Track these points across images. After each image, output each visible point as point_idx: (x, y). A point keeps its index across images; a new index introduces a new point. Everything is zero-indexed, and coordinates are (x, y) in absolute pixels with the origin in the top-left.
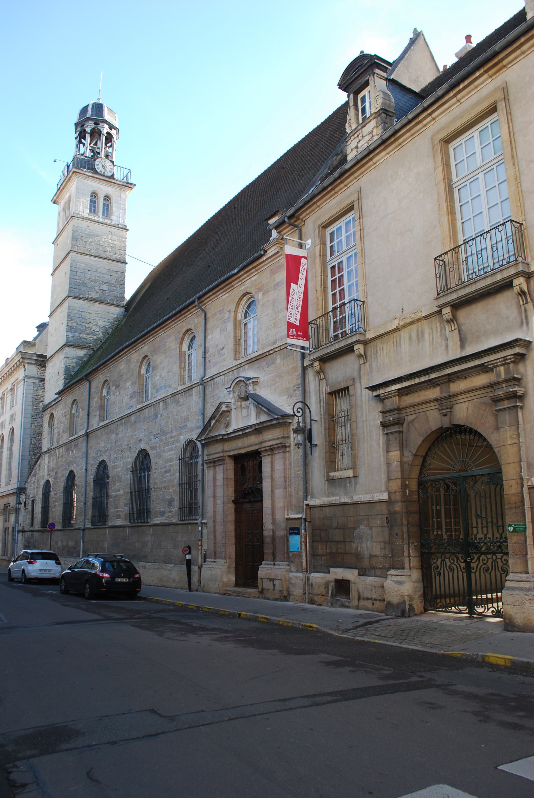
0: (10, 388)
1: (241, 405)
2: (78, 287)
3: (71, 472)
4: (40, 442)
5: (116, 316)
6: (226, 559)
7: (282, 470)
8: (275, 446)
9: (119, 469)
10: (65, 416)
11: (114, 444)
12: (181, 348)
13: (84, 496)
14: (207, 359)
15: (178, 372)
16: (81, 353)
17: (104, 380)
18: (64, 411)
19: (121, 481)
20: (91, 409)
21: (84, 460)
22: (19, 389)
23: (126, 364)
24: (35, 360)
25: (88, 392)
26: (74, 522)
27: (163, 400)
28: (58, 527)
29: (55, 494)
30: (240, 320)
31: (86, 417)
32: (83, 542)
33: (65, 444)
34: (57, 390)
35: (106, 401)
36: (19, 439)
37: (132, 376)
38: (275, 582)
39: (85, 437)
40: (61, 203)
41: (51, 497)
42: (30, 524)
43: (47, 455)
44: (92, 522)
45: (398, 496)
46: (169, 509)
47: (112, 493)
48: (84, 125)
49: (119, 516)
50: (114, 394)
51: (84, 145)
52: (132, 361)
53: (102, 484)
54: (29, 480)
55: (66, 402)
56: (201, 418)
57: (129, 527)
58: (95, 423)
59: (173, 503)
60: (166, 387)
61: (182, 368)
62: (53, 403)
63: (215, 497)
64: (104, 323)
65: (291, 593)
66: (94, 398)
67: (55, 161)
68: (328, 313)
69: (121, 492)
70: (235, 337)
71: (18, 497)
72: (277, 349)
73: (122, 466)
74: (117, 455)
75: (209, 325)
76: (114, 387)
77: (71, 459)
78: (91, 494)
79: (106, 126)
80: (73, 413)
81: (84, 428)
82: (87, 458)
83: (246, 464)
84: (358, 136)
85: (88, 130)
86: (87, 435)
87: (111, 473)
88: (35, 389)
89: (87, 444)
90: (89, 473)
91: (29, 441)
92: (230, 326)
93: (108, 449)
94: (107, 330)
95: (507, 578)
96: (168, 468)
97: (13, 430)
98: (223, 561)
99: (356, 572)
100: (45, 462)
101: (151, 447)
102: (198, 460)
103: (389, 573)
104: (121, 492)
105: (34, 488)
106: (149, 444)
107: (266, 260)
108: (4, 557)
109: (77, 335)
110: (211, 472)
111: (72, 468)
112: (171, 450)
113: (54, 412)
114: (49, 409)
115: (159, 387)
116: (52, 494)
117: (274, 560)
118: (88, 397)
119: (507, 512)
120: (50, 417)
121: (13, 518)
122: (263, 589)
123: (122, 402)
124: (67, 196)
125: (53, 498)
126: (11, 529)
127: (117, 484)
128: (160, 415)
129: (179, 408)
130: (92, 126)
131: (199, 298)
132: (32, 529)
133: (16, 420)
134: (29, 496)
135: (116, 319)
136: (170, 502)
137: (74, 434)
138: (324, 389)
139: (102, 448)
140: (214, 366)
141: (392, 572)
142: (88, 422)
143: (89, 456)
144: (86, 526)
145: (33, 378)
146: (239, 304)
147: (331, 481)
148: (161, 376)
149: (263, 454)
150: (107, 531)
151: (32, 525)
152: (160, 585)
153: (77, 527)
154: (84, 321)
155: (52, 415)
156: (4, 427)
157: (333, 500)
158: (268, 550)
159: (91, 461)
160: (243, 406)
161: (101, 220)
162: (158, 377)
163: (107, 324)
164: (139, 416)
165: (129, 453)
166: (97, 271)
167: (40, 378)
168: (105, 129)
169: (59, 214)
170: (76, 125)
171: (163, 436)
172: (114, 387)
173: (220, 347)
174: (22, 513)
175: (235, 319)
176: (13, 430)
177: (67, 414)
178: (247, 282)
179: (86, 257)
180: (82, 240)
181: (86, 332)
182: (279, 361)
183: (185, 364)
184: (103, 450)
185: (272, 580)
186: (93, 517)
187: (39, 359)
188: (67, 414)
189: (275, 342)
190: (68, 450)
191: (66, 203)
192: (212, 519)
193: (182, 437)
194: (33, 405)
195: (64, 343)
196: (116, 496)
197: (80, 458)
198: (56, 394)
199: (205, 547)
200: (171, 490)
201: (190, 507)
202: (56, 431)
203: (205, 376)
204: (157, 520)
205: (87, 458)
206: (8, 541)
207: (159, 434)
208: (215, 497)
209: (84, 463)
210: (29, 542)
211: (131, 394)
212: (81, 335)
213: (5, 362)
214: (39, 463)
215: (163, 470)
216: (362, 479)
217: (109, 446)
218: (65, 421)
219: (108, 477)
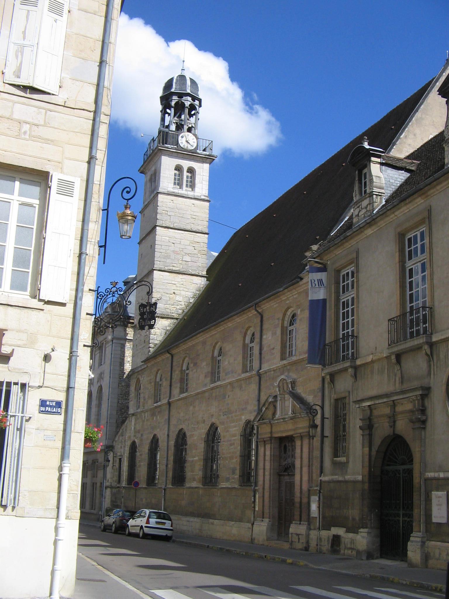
2: (163, 260)
3: (155, 436)
4: (126, 401)
10: (151, 383)
13: (166, 459)
15: (241, 361)
18: (149, 378)
21: (167, 426)
22: (107, 349)
25: (170, 365)
26: (157, 482)
27: (231, 384)
28: (143, 485)
29: (141, 455)
30: (287, 327)
31: (169, 387)
32: (164, 500)
38: (300, 536)
39: (168, 406)
43: (134, 418)
44: (172, 483)
45: (366, 479)
47: (189, 459)
49: (194, 480)
50: (192, 370)
51: (169, 114)
53: (182, 449)
54: (116, 439)
56: (257, 403)
60: (232, 373)
61: (244, 358)
62: (140, 369)
63: (264, 469)
71: (106, 453)
75: (265, 326)
78: (171, 458)
79: (189, 99)
80: (157, 380)
82: (169, 424)
83: (287, 445)
84: (359, 207)
87: (189, 441)
90: (171, 438)
92: (279, 331)
94: (189, 300)
95: (411, 535)
97: (100, 388)
99: (344, 529)
100: (132, 424)
103: (359, 530)
105: (121, 447)
108: (92, 511)
111: (155, 432)
112: (235, 427)
114: (136, 374)
116: (138, 454)
117: (300, 520)
118: (170, 368)
119: (414, 494)
121: (100, 474)
122: (292, 541)
124: (153, 169)
126: (98, 485)
127: (194, 451)
128: (227, 396)
133: (105, 379)
134: (116, 454)
141: (361, 530)
143: (171, 424)
147: (335, 464)
148: (229, 363)
153: (159, 486)
155: (138, 381)
157: (336, 478)
158: (297, 513)
159: (172, 427)
165: (203, 425)
166: (180, 243)
169: (146, 185)
170: (162, 98)
173: (272, 347)
174: (109, 469)
175: (282, 327)
176: (100, 388)
179: (170, 230)
180: (167, 214)
181: (170, 302)
185: (298, 535)
190: (153, 415)
193: (243, 417)
196: (193, 461)
198: (142, 362)
200: (234, 460)
202: (142, 395)
203: (260, 369)
204: (224, 485)
205: (169, 424)
208: (264, 469)
209: (166, 429)
210: (116, 498)
216: (351, 465)
219: (186, 445)
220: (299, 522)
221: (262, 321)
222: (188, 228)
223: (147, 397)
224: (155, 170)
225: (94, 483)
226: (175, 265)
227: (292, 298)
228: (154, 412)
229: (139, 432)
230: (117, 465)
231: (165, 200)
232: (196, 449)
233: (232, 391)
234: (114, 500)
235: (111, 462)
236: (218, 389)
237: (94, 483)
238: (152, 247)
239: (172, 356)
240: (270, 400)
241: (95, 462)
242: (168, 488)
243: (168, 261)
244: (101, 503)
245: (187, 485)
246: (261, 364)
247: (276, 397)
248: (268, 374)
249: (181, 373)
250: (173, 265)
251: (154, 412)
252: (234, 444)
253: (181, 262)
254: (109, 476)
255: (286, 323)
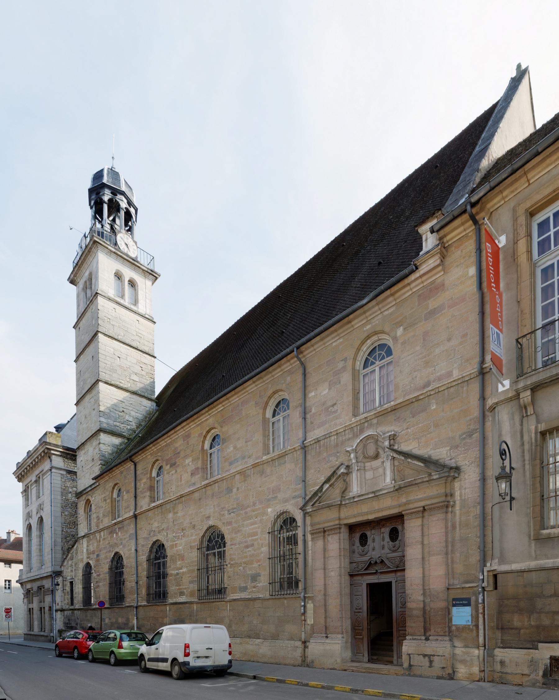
0: (34, 479)
1: (364, 467)
5: (148, 409)
6: (342, 634)
7: (444, 534)
8: (430, 507)
9: (181, 548)
10: (105, 500)
11: (171, 524)
12: (264, 414)
13: (135, 576)
14: (308, 421)
16: (117, 441)
17: (155, 459)
18: (103, 496)
19: (183, 560)
20: (138, 491)
22: (45, 480)
23: (184, 441)
24: (61, 452)
27: (240, 473)
30: (359, 370)
32: (137, 618)
33: (107, 528)
34: (94, 476)
35: (156, 482)
36: (50, 526)
37: (192, 451)
39: (134, 519)
40: (80, 283)
41: (92, 578)
42: (70, 603)
43: (85, 540)
46: (253, 584)
48: (100, 193)
50: (168, 473)
52: (192, 436)
55: (105, 487)
57: (197, 603)
58: (144, 504)
59: (258, 578)
60: (243, 458)
62: (89, 489)
64: (137, 414)
65: (455, 670)
66: (141, 480)
67: (71, 229)
68: (534, 332)
69: (184, 570)
70: (354, 389)
72: (432, 393)
73: (183, 545)
74: (176, 533)
75: (310, 381)
76: (169, 466)
77: (115, 541)
81: (130, 510)
85: (106, 198)
86: (135, 516)
88: (63, 480)
89: (136, 526)
90: (140, 553)
91: (60, 529)
92: (346, 377)
93: (163, 529)
96: (249, 543)
97: (41, 519)
98: (340, 636)
100: (83, 546)
101: (223, 523)
102: (297, 532)
104: (184, 570)
105: (72, 571)
106: (220, 520)
107: (421, 277)
109: (111, 422)
110: (320, 543)
113: (90, 498)
114: (84, 496)
115: (233, 459)
118: (133, 479)
120: (86, 503)
121: (48, 599)
123: (179, 480)
124: (87, 274)
125: (96, 579)
126: (47, 609)
127: (179, 563)
129: (264, 479)
130: (107, 200)
131: (298, 348)
132: (72, 607)
133: (45, 510)
135: (150, 413)
136: (255, 578)
137: (117, 517)
138: (533, 427)
139: (154, 529)
140: (319, 427)
142: (136, 504)
143: (138, 537)
144: (139, 604)
145: (61, 469)
146: (359, 350)
148: (235, 447)
149: (405, 518)
150: (168, 608)
151: (72, 604)
152: (243, 659)
153: (127, 605)
154: (117, 409)
155: (88, 502)
156: (31, 517)
159: (141, 542)
160: (366, 468)
161: (126, 304)
162: (232, 449)
163: (140, 416)
164: (206, 492)
166: (126, 359)
167: (67, 470)
168: (124, 204)
170: (91, 191)
171: (242, 510)
172: (169, 466)
173: (330, 403)
175: (354, 369)
176: (41, 519)
177: (107, 498)
178: (376, 318)
182: (434, 407)
183: (269, 432)
184: (157, 529)
186: (148, 595)
187: (65, 451)
188: (107, 498)
189: (428, 384)
190: (111, 533)
191: (86, 282)
192: (322, 593)
193: (269, 510)
194: (62, 495)
195: (98, 428)
196: (178, 574)
197: (127, 539)
198: (93, 479)
199: (310, 621)
201: (289, 582)
202: (94, 516)
203: (305, 440)
206: (45, 619)
207: (235, 508)
210: (69, 620)
211: (192, 471)
212: (115, 423)
213: (26, 454)
214: (75, 547)
215: (242, 545)
217: (164, 526)
218: (106, 506)
219: (165, 557)
220: (423, 638)
221: (305, 374)
222: (134, 345)
223: (101, 515)
224: (91, 274)
225: (41, 608)
226: (123, 382)
227: (380, 316)
228: (111, 529)
229: (93, 553)
230: (68, 589)
231: (106, 305)
232: (183, 560)
233: (245, 481)
234: (68, 622)
235: (60, 586)
236: (216, 484)
237: (41, 608)
238: (95, 358)
239: (135, 465)
240: (342, 470)
241: (41, 589)
242: (141, 606)
243: (114, 375)
244: (52, 625)
245: (170, 601)
246: (305, 433)
247: (348, 467)
248: (322, 442)
249: (151, 480)
250: (121, 381)
251: (111, 529)
252: (253, 545)
253: (128, 380)
254: (58, 598)
255: (358, 363)
